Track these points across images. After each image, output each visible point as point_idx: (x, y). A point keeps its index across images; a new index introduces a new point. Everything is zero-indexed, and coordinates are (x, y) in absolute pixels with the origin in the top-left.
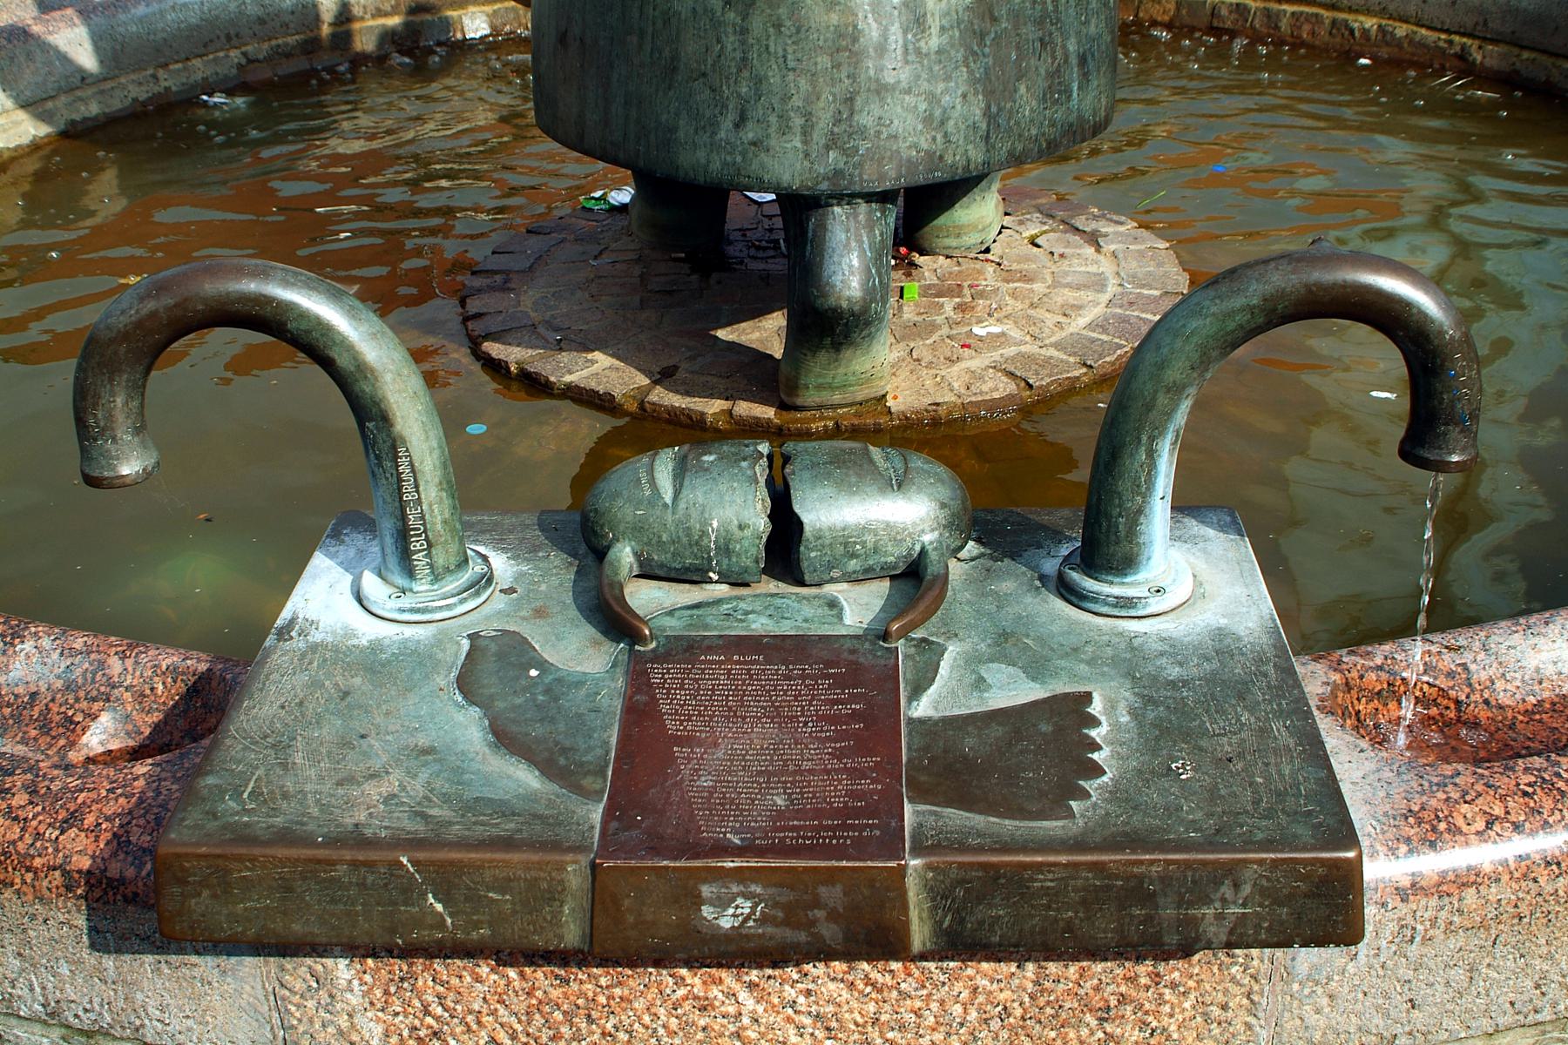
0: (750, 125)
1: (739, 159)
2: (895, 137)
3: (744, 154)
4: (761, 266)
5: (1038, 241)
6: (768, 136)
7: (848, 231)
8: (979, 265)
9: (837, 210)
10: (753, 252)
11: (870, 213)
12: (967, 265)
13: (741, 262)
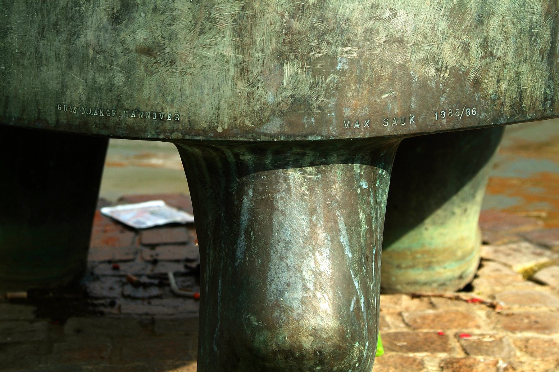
0: (140, 17)
1: (119, 79)
2: (400, 41)
3: (128, 70)
4: (139, 308)
5: (541, 275)
6: (173, 37)
7: (312, 212)
8: (462, 307)
9: (294, 174)
10: (129, 290)
11: (351, 182)
12: (443, 306)
13: (112, 304)
